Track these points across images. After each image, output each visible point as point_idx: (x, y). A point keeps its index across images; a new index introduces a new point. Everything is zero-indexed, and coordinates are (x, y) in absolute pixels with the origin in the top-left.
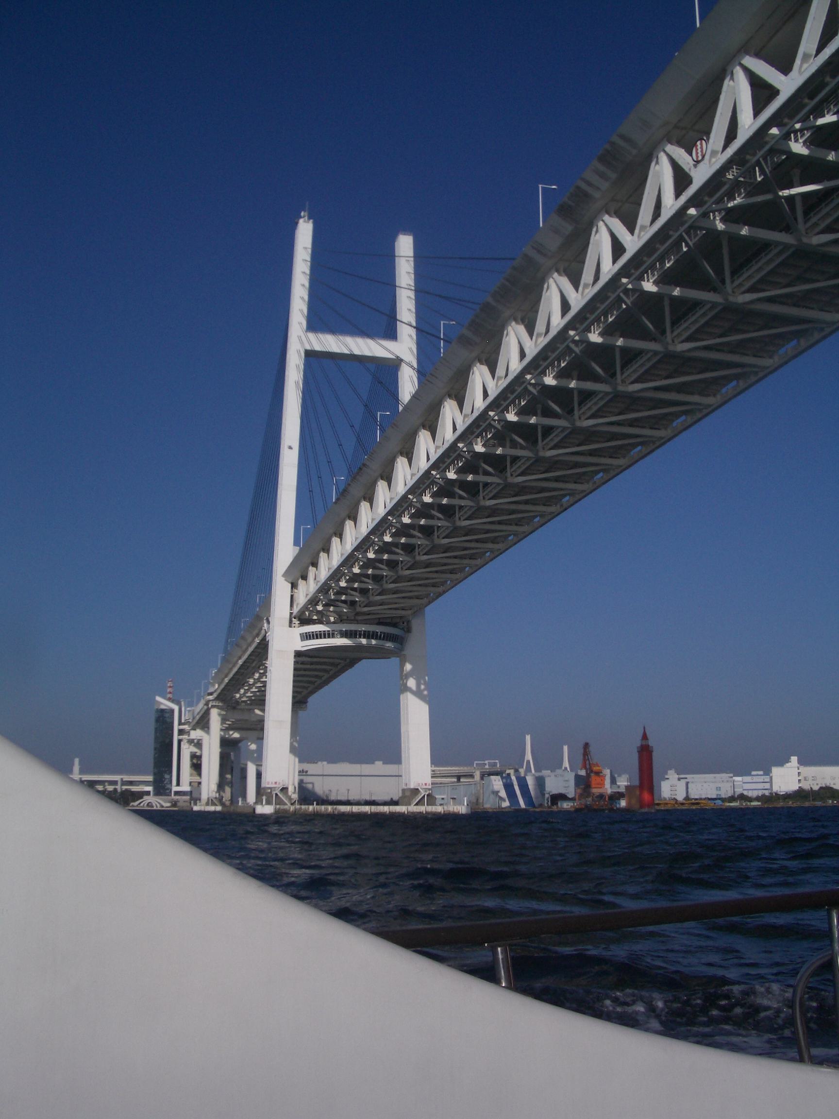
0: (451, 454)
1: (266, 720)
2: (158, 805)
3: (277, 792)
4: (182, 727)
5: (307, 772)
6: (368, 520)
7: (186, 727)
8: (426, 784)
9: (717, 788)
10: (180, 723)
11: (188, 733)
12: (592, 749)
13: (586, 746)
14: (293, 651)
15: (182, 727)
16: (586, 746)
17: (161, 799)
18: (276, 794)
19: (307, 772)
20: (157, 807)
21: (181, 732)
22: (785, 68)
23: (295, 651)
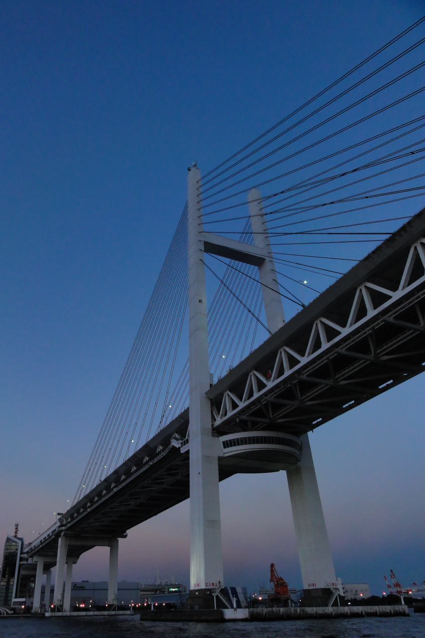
0: (352, 337)
1: (65, 558)
2: (5, 613)
3: (217, 593)
4: (22, 556)
5: (84, 587)
6: (34, 542)
7: (26, 556)
8: (213, 584)
9: (309, 584)
10: (21, 553)
11: (27, 560)
12: (276, 567)
13: (272, 565)
14: (217, 457)
15: (22, 556)
16: (272, 565)
17: (6, 608)
18: (217, 597)
19: (84, 587)
20: (4, 614)
21: (21, 559)
22: (303, 355)
23: (219, 457)
